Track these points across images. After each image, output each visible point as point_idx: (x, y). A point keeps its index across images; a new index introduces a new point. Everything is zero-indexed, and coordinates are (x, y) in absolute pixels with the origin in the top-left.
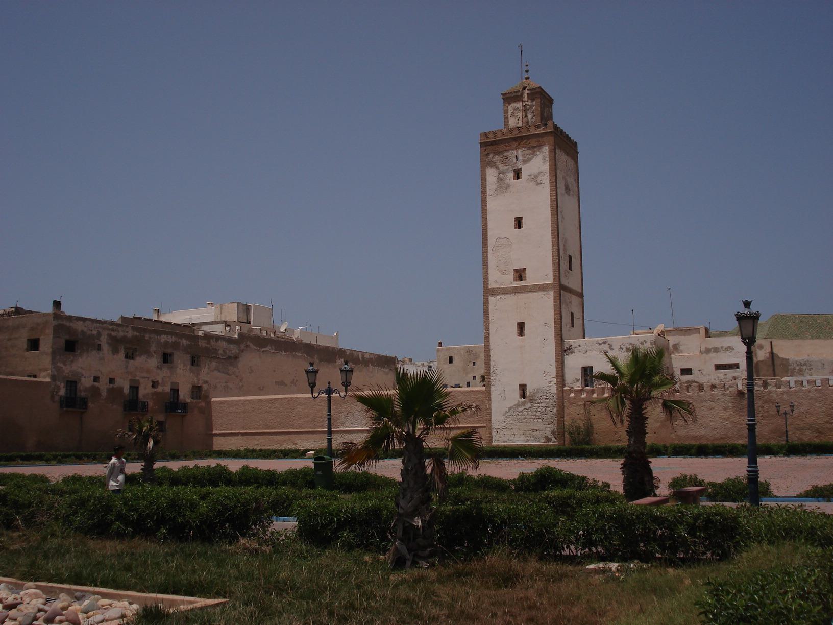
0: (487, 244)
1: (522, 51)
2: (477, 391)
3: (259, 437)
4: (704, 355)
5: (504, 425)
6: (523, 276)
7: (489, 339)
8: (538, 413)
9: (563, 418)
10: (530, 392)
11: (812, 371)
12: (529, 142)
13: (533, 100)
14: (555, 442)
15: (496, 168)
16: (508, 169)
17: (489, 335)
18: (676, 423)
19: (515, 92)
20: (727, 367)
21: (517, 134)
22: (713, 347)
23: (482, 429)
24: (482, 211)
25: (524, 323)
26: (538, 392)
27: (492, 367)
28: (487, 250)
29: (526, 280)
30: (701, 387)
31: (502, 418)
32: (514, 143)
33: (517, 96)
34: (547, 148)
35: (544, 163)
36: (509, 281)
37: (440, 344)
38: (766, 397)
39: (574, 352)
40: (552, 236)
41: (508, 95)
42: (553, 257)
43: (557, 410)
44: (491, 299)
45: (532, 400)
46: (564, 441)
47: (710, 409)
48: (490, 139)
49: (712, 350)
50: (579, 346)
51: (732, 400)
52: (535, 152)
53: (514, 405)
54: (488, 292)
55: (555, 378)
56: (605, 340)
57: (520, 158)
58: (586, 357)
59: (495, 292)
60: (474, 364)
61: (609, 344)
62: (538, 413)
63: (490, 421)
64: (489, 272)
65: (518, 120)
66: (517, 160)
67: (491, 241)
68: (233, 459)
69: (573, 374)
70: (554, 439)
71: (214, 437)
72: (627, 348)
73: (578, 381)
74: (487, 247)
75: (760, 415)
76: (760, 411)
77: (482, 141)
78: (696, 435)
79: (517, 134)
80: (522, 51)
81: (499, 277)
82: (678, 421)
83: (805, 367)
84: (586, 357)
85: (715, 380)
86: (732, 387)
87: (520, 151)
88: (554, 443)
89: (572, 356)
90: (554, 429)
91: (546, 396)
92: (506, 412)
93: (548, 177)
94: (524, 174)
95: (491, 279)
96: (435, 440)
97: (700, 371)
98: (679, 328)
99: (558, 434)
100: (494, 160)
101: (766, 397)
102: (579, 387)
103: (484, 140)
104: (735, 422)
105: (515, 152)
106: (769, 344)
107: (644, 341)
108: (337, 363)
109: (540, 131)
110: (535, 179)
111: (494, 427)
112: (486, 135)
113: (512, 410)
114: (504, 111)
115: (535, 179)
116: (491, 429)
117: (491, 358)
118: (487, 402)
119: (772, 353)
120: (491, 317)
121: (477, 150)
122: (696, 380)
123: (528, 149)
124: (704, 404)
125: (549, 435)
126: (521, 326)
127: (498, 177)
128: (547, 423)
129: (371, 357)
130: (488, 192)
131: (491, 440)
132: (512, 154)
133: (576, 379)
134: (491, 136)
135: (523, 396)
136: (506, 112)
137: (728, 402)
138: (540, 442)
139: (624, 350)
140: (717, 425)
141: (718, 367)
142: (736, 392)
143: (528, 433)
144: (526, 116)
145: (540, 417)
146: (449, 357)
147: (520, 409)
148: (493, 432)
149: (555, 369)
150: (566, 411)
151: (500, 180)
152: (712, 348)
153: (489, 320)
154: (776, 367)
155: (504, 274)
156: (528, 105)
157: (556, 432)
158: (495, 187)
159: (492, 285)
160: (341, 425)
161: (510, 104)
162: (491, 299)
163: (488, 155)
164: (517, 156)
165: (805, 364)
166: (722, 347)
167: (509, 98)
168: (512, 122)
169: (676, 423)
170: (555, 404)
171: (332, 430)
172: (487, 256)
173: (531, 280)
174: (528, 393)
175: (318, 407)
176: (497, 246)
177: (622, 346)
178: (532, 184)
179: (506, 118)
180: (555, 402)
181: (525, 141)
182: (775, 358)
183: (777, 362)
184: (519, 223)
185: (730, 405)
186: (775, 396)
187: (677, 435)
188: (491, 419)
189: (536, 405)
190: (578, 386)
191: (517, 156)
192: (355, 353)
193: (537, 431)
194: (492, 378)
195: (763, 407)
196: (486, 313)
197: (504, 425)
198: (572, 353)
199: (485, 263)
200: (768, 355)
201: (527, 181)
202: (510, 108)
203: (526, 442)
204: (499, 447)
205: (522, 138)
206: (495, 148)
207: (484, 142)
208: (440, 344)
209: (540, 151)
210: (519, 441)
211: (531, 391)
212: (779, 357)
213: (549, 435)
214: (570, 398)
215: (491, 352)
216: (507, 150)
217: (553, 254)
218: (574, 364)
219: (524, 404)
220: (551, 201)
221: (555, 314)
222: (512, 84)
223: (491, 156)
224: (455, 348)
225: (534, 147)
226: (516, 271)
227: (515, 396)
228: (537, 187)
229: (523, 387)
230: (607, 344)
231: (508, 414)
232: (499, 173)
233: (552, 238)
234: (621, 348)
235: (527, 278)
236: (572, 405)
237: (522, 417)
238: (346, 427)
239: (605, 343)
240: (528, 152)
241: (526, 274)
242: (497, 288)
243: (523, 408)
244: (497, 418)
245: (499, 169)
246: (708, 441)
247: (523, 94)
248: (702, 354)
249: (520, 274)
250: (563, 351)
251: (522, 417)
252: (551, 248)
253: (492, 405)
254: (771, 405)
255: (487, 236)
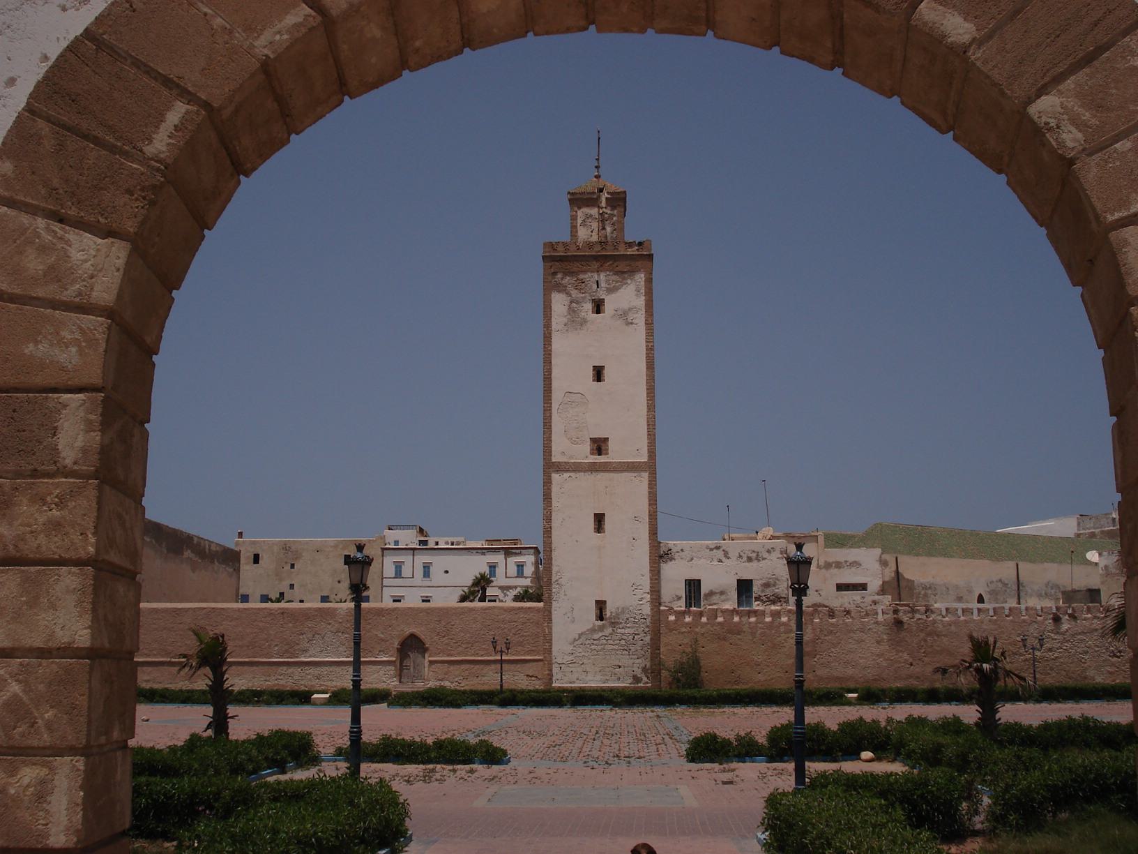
0: (551, 400)
1: (599, 138)
2: (529, 608)
3: (150, 669)
4: (823, 570)
5: (571, 657)
6: (603, 448)
7: (551, 534)
8: (623, 642)
9: (659, 649)
10: (611, 612)
11: (937, 597)
12: (616, 264)
13: (613, 208)
14: (647, 683)
15: (567, 293)
16: (585, 297)
17: (551, 527)
18: (815, 659)
19: (588, 193)
20: (851, 587)
21: (599, 251)
22: (834, 560)
23: (536, 663)
24: (544, 351)
25: (604, 514)
26: (623, 612)
27: (554, 575)
28: (551, 407)
29: (607, 454)
30: (832, 614)
31: (569, 648)
32: (595, 262)
33: (592, 199)
34: (643, 275)
35: (637, 295)
36: (583, 454)
37: (240, 534)
38: (929, 629)
39: (674, 559)
40: (647, 397)
41: (578, 196)
42: (648, 425)
43: (651, 639)
44: (555, 477)
45: (614, 624)
46: (660, 681)
47: (859, 641)
48: (559, 252)
49: (834, 565)
50: (682, 550)
51: (887, 631)
52: (624, 279)
53: (588, 630)
54: (550, 467)
55: (648, 593)
56: (719, 545)
57: (603, 284)
58: (691, 567)
59: (561, 468)
60: (293, 566)
61: (724, 550)
62: (623, 642)
63: (550, 651)
64: (553, 438)
65: (592, 232)
66: (598, 287)
67: (557, 396)
68: (181, 706)
69: (673, 589)
70: (645, 679)
71: (139, 668)
72: (748, 557)
73: (679, 598)
74: (551, 404)
75: (922, 651)
76: (923, 646)
77: (547, 254)
78: (842, 676)
79: (599, 251)
80: (599, 138)
81: (562, 449)
82: (818, 656)
83: (929, 592)
84: (691, 567)
85: (850, 603)
86: (887, 614)
87: (602, 276)
88: (646, 683)
89: (671, 564)
90: (646, 666)
91: (635, 618)
92: (575, 640)
93: (644, 315)
94: (609, 307)
95: (556, 448)
96: (462, 678)
97: (817, 591)
98: (790, 534)
99: (652, 673)
100: (563, 282)
101: (929, 629)
102: (681, 607)
103: (549, 252)
104: (892, 660)
105: (595, 276)
106: (894, 559)
107: (772, 548)
108: (184, 556)
109: (632, 251)
110: (624, 316)
111: (556, 660)
112: (551, 246)
113: (583, 638)
114: (571, 216)
115: (624, 316)
116: (550, 664)
117: (553, 562)
118: (546, 624)
119: (897, 572)
120: (554, 503)
121: (539, 267)
122: (826, 603)
123: (614, 274)
124: (852, 635)
125: (639, 673)
126: (599, 519)
127: (570, 308)
128: (636, 657)
129: (218, 549)
130: (554, 326)
131: (551, 679)
132: (590, 277)
133: (677, 596)
134: (560, 248)
135: (601, 617)
136: (574, 218)
137: (882, 633)
138: (625, 683)
139: (745, 559)
140: (869, 663)
141: (840, 587)
142: (893, 621)
143: (607, 669)
144: (604, 228)
145: (626, 648)
146: (255, 555)
147: (596, 636)
148: (554, 668)
149: (649, 581)
150: (663, 639)
151: (571, 311)
152: (833, 562)
153: (551, 506)
154: (901, 590)
155: (575, 443)
156: (607, 213)
157: (648, 670)
158: (565, 320)
159: (556, 458)
160: (301, 653)
161: (579, 208)
162: (555, 477)
163: (554, 274)
164: (597, 281)
165: (930, 588)
166: (846, 562)
167: (579, 200)
168: (583, 234)
169: (815, 659)
170: (647, 629)
171: (362, 659)
172: (551, 416)
173: (615, 454)
174: (608, 614)
175: (261, 624)
176: (566, 404)
177: (742, 554)
178: (620, 322)
179: (574, 228)
180: (647, 627)
181: (611, 262)
182: (900, 577)
183: (903, 584)
184: (598, 374)
185: (885, 637)
186: (941, 627)
187: (817, 676)
188: (551, 648)
189: (619, 631)
190: (680, 605)
191: (597, 281)
192: (202, 542)
193: (620, 667)
194: (554, 590)
195: (926, 641)
196: (547, 497)
197: (571, 657)
198: (671, 560)
199: (547, 426)
200: (893, 575)
201: (612, 317)
202: (581, 214)
203: (604, 683)
204: (583, 691)
205: (606, 258)
206: (566, 266)
207: (551, 256)
208: (240, 534)
209: (631, 279)
210: (593, 681)
211: (613, 610)
212: (904, 578)
213: (639, 673)
214: (668, 622)
215: (553, 553)
216: (585, 272)
217: (648, 422)
218: (674, 576)
219: (601, 629)
220: (647, 350)
221: (650, 505)
222: (586, 183)
223: (559, 276)
224: (264, 541)
225: (623, 272)
226: (594, 440)
227: (589, 617)
228: (627, 327)
229: (601, 605)
230: (721, 549)
231: (577, 643)
232: (571, 302)
233: (648, 400)
234: (740, 556)
235: (609, 452)
236: (671, 632)
237: (599, 647)
238: (310, 656)
239: (718, 548)
240: (615, 277)
241: (608, 446)
242: (565, 462)
243: (600, 634)
244: (561, 647)
245: (570, 296)
246: (857, 683)
247: (599, 197)
248: (820, 569)
249: (599, 446)
250: (660, 556)
251: (599, 647)
252: (646, 414)
253: (553, 628)
254: (936, 638)
255: (551, 387)
